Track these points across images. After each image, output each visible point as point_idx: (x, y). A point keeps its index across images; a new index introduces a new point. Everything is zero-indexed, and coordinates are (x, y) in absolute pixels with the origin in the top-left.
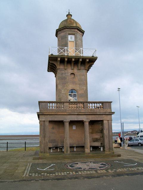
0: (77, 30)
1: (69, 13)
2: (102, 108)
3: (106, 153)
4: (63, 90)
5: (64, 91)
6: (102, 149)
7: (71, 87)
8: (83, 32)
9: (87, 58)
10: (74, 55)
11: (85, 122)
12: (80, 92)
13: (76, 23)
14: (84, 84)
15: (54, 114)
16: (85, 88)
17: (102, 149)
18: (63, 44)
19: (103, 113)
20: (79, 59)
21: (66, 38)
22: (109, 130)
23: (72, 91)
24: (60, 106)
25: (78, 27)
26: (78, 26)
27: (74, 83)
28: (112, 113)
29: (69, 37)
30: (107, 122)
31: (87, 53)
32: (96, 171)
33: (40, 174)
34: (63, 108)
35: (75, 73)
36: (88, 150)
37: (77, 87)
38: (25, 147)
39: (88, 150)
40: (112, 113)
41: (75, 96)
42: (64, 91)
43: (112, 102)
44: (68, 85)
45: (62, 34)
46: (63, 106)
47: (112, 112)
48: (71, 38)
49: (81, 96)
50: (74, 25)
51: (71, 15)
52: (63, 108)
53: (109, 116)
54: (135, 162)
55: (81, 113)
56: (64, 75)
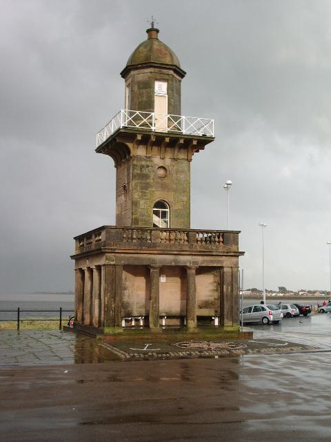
0: (171, 72)
1: (152, 24)
2: (221, 243)
3: (225, 328)
4: (143, 201)
5: (146, 203)
6: (217, 322)
7: (158, 195)
8: (182, 74)
9: (194, 138)
10: (166, 130)
11: (190, 268)
12: (177, 207)
13: (171, 55)
14: (184, 192)
15: (133, 252)
16: (185, 199)
17: (217, 322)
18: (142, 101)
19: (224, 252)
20: (178, 139)
21: (148, 86)
22: (232, 285)
23: (160, 204)
24: (144, 237)
25: (176, 66)
26: (175, 64)
27: (164, 187)
28: (238, 254)
29: (157, 84)
30: (229, 270)
31: (189, 127)
32: (229, 351)
33: (147, 354)
34: (149, 241)
35: (167, 168)
36: (192, 324)
37: (168, 197)
38: (18, 321)
39: (192, 324)
40: (238, 254)
41: (164, 215)
42: (146, 203)
43: (240, 232)
44: (153, 191)
45: (141, 75)
46: (149, 237)
47: (240, 251)
48: (161, 88)
49: (178, 215)
50: (167, 60)
51: (157, 31)
52: (149, 241)
53: (234, 259)
54: (284, 342)
55: (184, 251)
56: (145, 171)
